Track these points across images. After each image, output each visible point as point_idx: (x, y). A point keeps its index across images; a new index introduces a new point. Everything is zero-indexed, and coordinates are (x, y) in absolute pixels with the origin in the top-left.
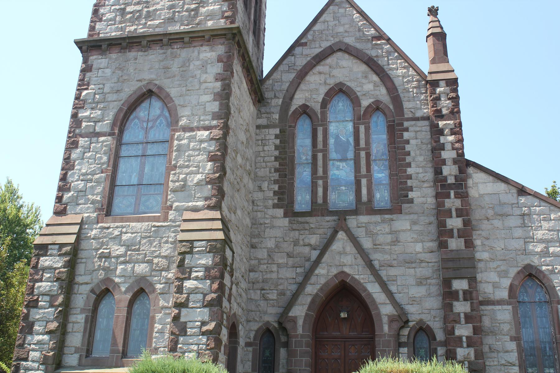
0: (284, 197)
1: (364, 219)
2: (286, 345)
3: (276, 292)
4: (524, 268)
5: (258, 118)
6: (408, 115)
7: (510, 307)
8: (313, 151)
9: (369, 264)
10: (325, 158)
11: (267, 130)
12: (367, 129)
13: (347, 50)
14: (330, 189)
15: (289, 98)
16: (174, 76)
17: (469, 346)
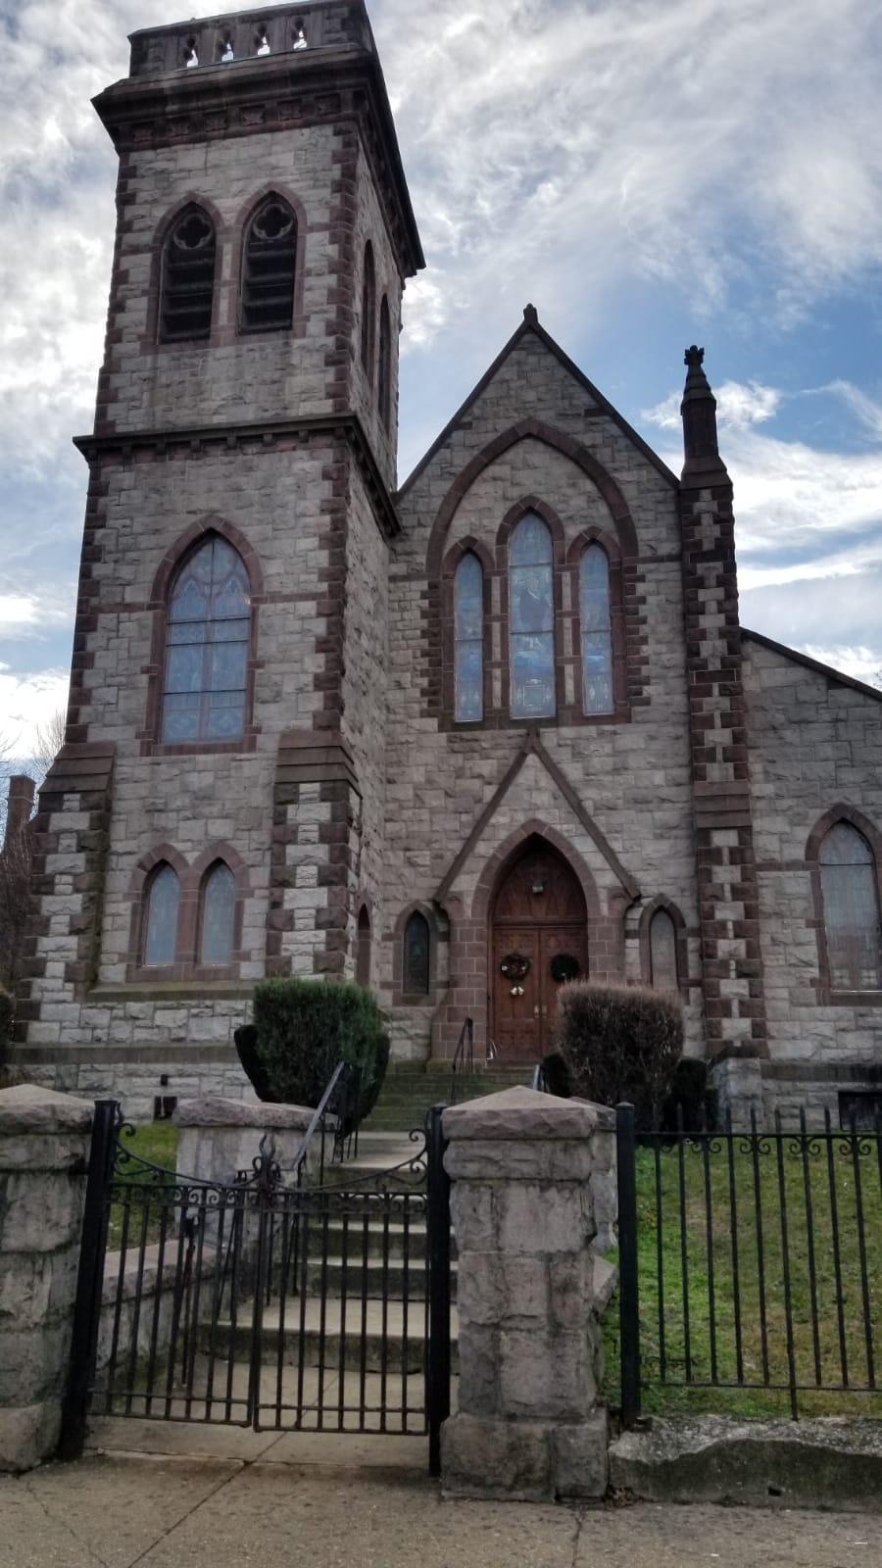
1: (567, 732)
4: (833, 810)
6: (644, 551)
7: (807, 874)
9: (578, 808)
12: (575, 579)
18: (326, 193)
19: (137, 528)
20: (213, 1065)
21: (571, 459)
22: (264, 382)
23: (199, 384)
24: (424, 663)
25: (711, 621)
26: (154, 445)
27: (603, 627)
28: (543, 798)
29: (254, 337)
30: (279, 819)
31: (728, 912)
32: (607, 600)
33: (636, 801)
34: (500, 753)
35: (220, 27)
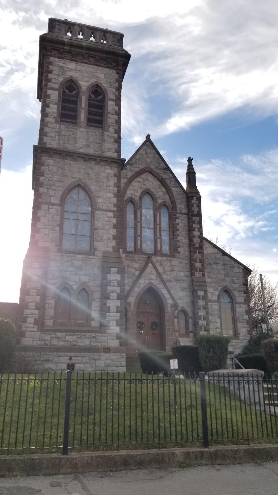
1: (159, 258)
6: (178, 211)
7: (218, 304)
12: (160, 215)
13: (151, 172)
17: (204, 320)
18: (114, 90)
19: (55, 179)
20: (86, 354)
21: (159, 181)
22: (96, 143)
23: (75, 138)
25: (196, 233)
26: (61, 154)
27: (166, 230)
28: (153, 277)
29: (93, 128)
31: (202, 313)
32: (168, 222)
33: (176, 280)
34: (140, 262)
35: (80, 27)
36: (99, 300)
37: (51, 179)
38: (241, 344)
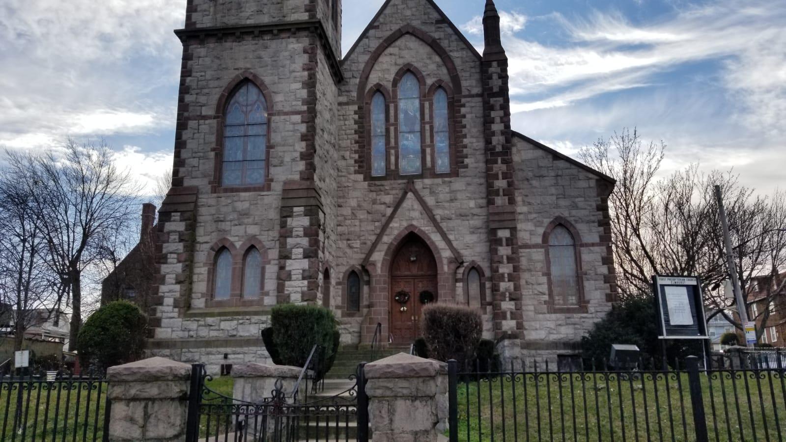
0: (363, 164)
1: (427, 181)
2: (368, 283)
3: (358, 241)
5: (339, 95)
7: (543, 250)
8: (386, 126)
9: (432, 219)
10: (396, 130)
11: (347, 107)
12: (431, 105)
14: (400, 157)
15: (365, 78)
16: (267, 66)
17: (509, 281)
20: (250, 348)
24: (356, 147)
25: (497, 127)
27: (444, 130)
28: (416, 214)
30: (283, 225)
31: (505, 269)
32: (446, 116)
33: (461, 215)
34: (394, 192)
36: (277, 262)
37: (203, 78)
38: (591, 321)
